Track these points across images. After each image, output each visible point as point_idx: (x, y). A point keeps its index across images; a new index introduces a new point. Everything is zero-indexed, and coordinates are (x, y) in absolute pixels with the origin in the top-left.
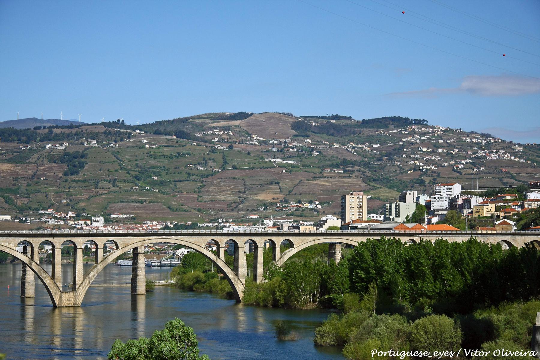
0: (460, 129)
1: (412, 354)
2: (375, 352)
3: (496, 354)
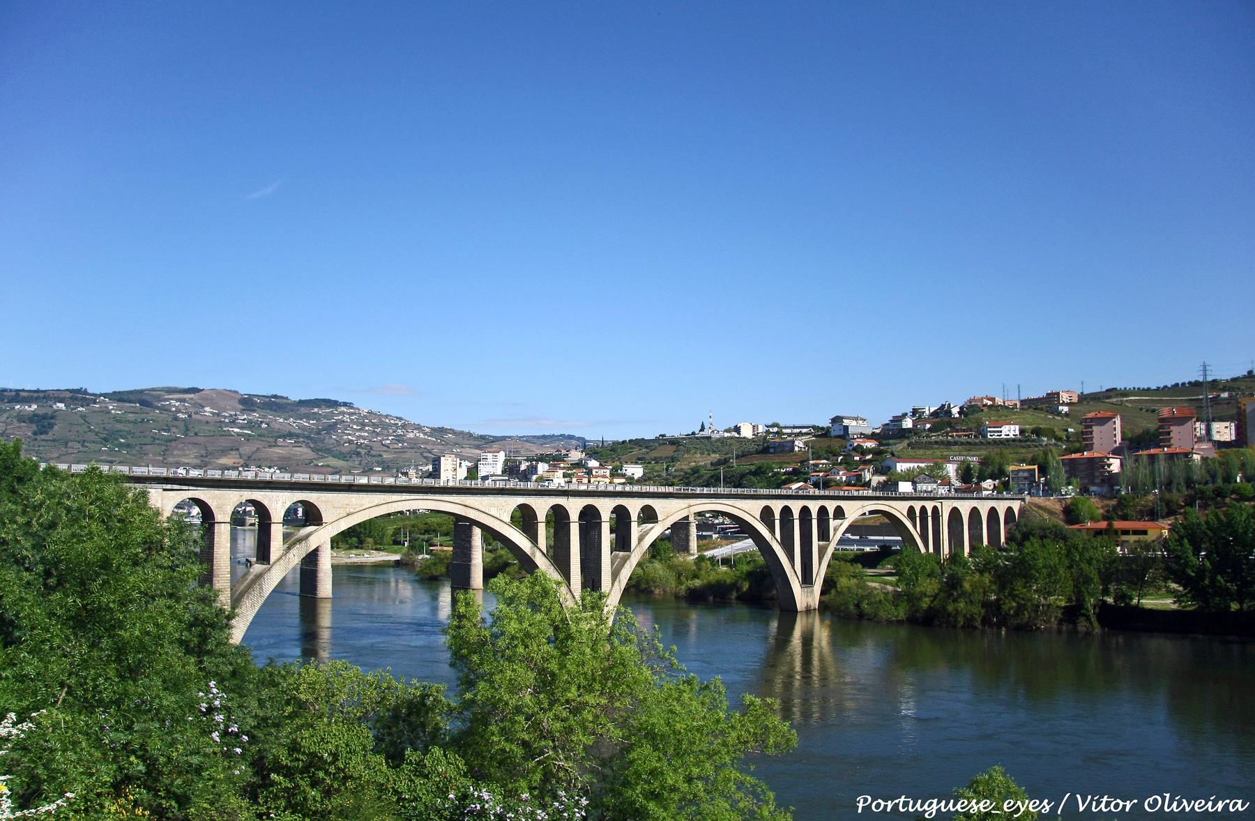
1: (921, 807)
2: (865, 800)
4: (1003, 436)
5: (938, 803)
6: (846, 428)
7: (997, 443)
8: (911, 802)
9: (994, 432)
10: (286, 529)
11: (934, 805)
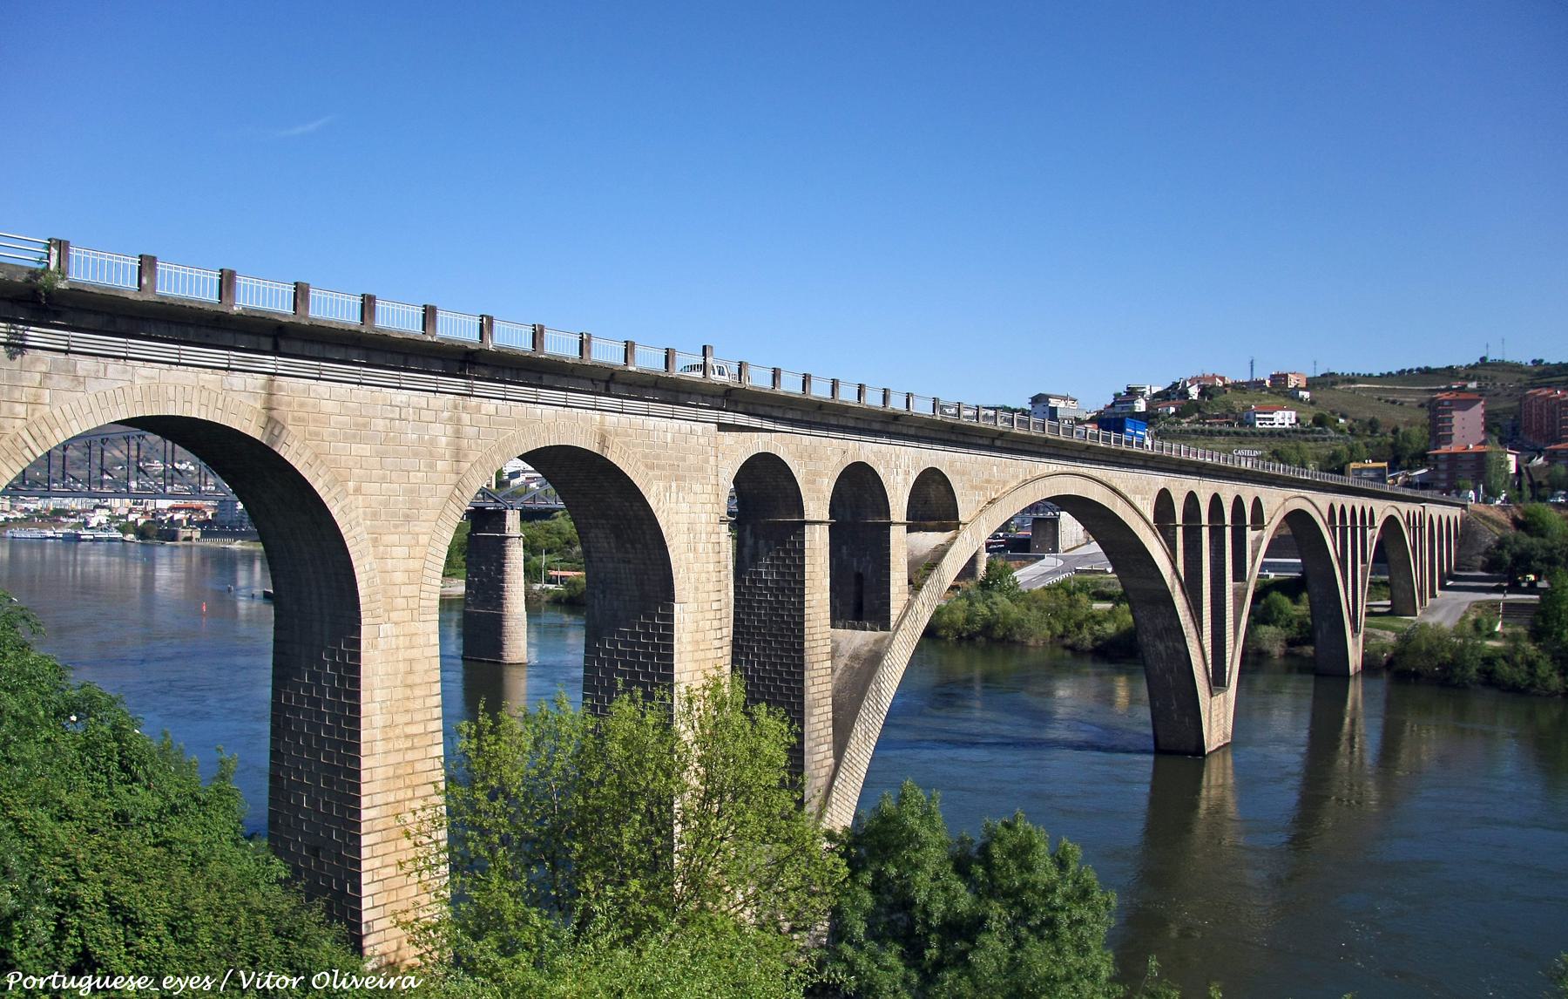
0: (1222, 379)
1: (75, 983)
2: (17, 977)
3: (28, 985)
4: (1276, 426)
5: (94, 980)
6: (1054, 410)
7: (1272, 433)
8: (65, 979)
9: (1264, 419)
10: (242, 544)
11: (89, 982)
